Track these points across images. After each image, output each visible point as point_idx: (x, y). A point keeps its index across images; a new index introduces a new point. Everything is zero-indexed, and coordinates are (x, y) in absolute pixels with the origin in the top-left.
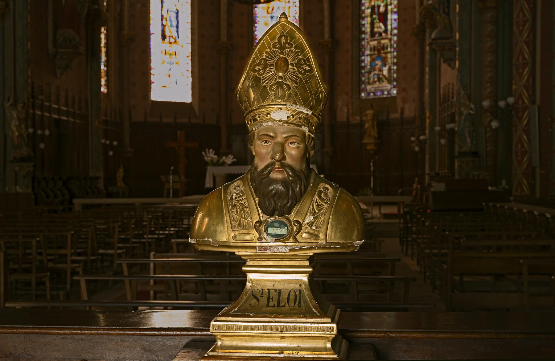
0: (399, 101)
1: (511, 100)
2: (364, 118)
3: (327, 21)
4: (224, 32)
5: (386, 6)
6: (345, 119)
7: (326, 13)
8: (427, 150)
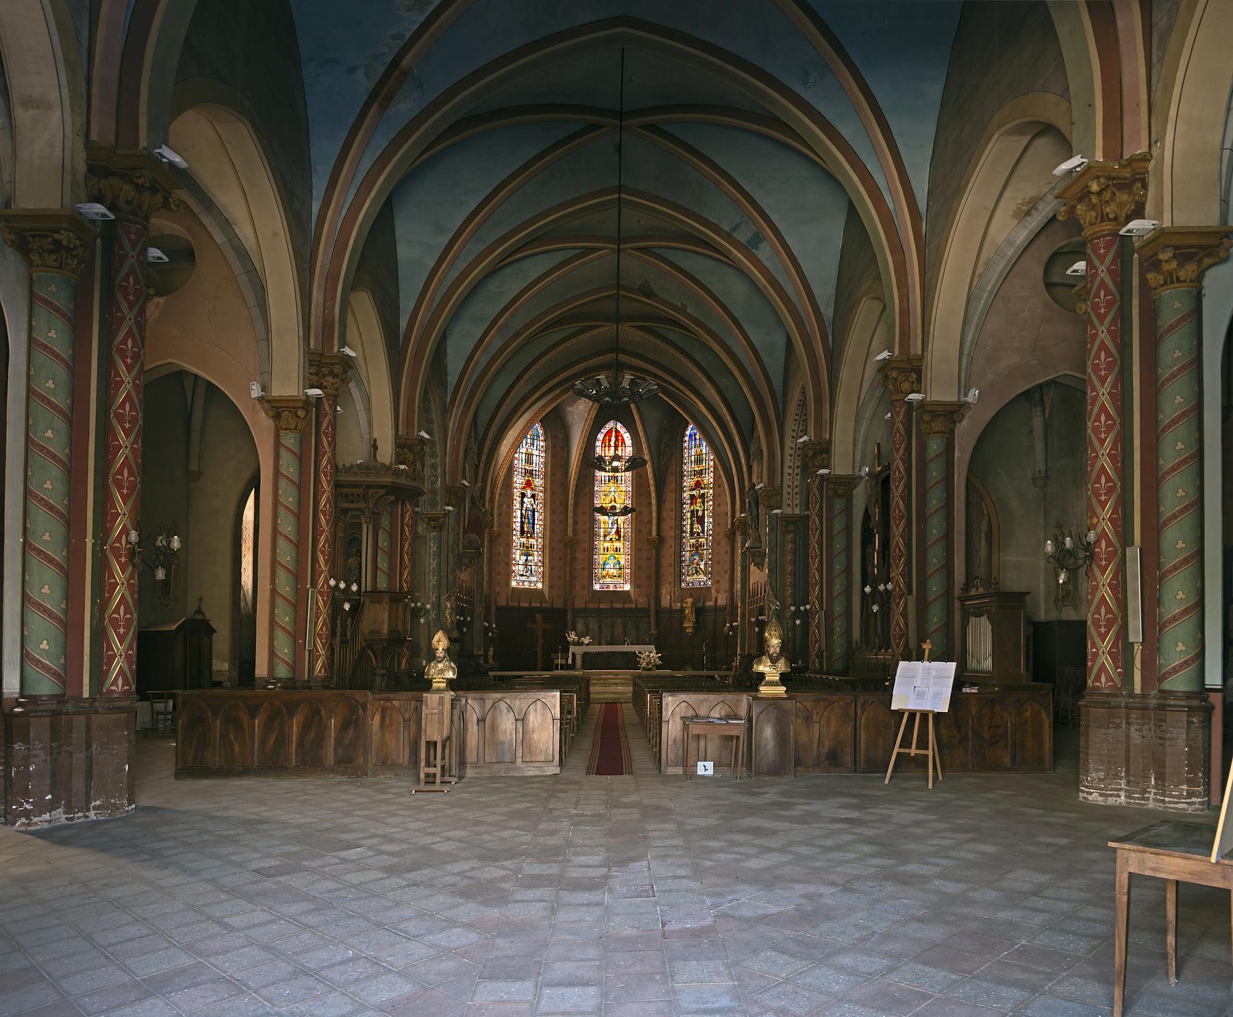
0: (713, 591)
1: (808, 607)
2: (684, 605)
3: (654, 521)
4: (570, 528)
5: (704, 511)
6: (668, 605)
7: (654, 515)
8: (739, 634)
